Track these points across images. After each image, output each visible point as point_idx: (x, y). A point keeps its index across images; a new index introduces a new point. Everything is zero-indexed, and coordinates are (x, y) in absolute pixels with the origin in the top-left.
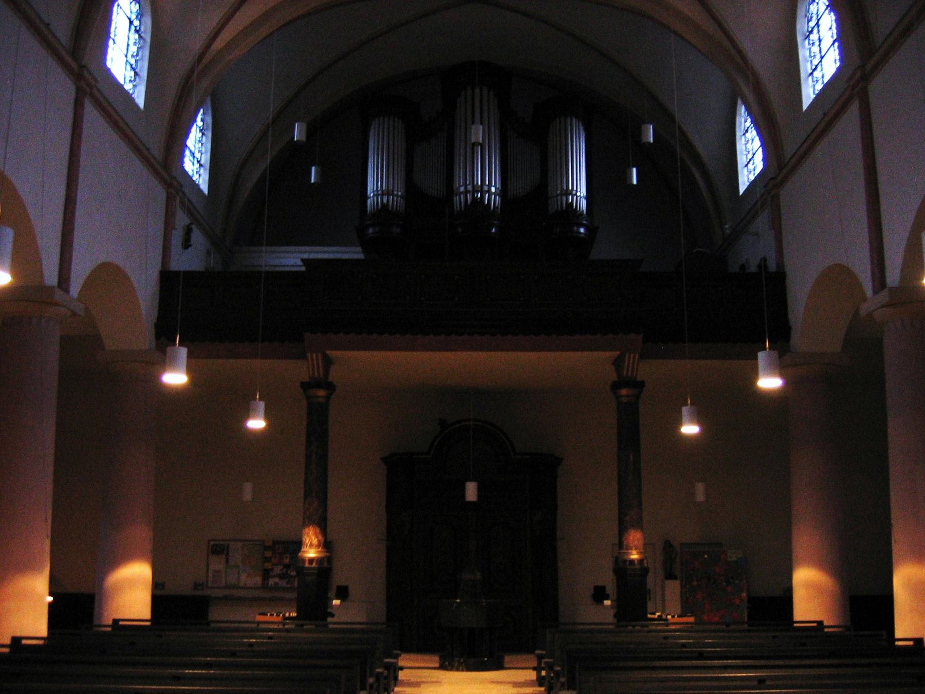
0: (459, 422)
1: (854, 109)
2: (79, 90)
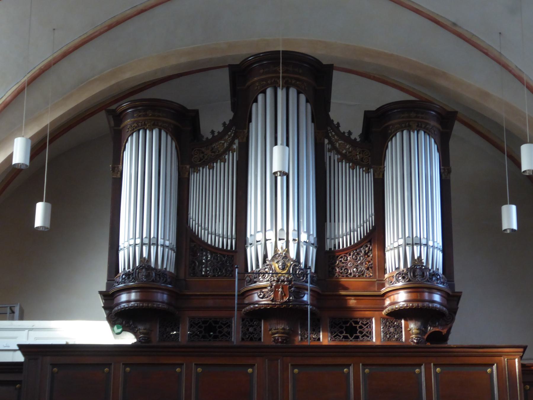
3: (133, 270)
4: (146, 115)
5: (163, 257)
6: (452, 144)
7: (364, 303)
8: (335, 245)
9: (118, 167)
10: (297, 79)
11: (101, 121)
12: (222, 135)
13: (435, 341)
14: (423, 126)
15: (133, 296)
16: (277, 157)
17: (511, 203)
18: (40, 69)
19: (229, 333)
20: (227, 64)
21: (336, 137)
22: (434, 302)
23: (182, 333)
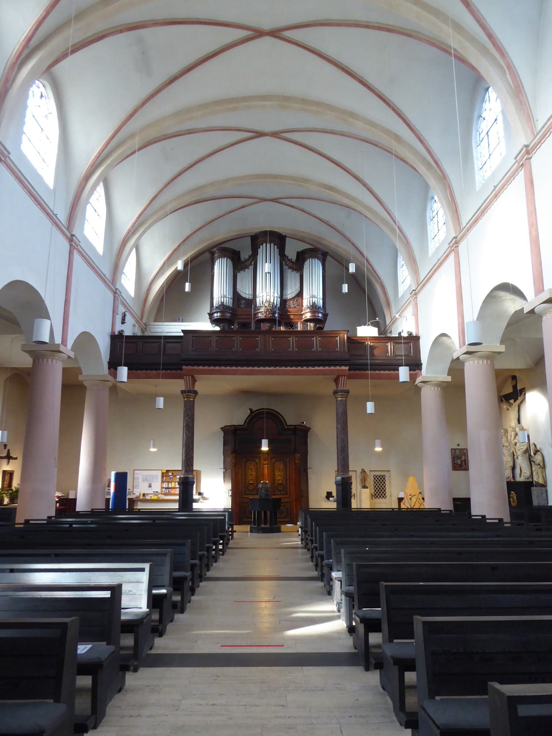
0: (277, 412)
1: (521, 176)
2: (71, 245)
5: (228, 302)
6: (327, 263)
7: (295, 317)
11: (207, 255)
12: (248, 260)
13: (319, 330)
15: (219, 314)
16: (267, 267)
19: (251, 327)
23: (235, 327)
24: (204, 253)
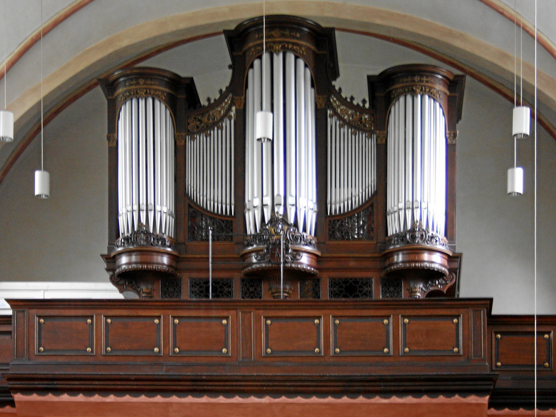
3: (131, 235)
4: (138, 84)
8: (340, 208)
9: (113, 137)
10: (294, 44)
12: (218, 102)
14: (427, 90)
15: (134, 258)
17: (518, 166)
18: (32, 39)
20: (221, 30)
21: (337, 103)
22: (163, 264)
24: (89, 88)
